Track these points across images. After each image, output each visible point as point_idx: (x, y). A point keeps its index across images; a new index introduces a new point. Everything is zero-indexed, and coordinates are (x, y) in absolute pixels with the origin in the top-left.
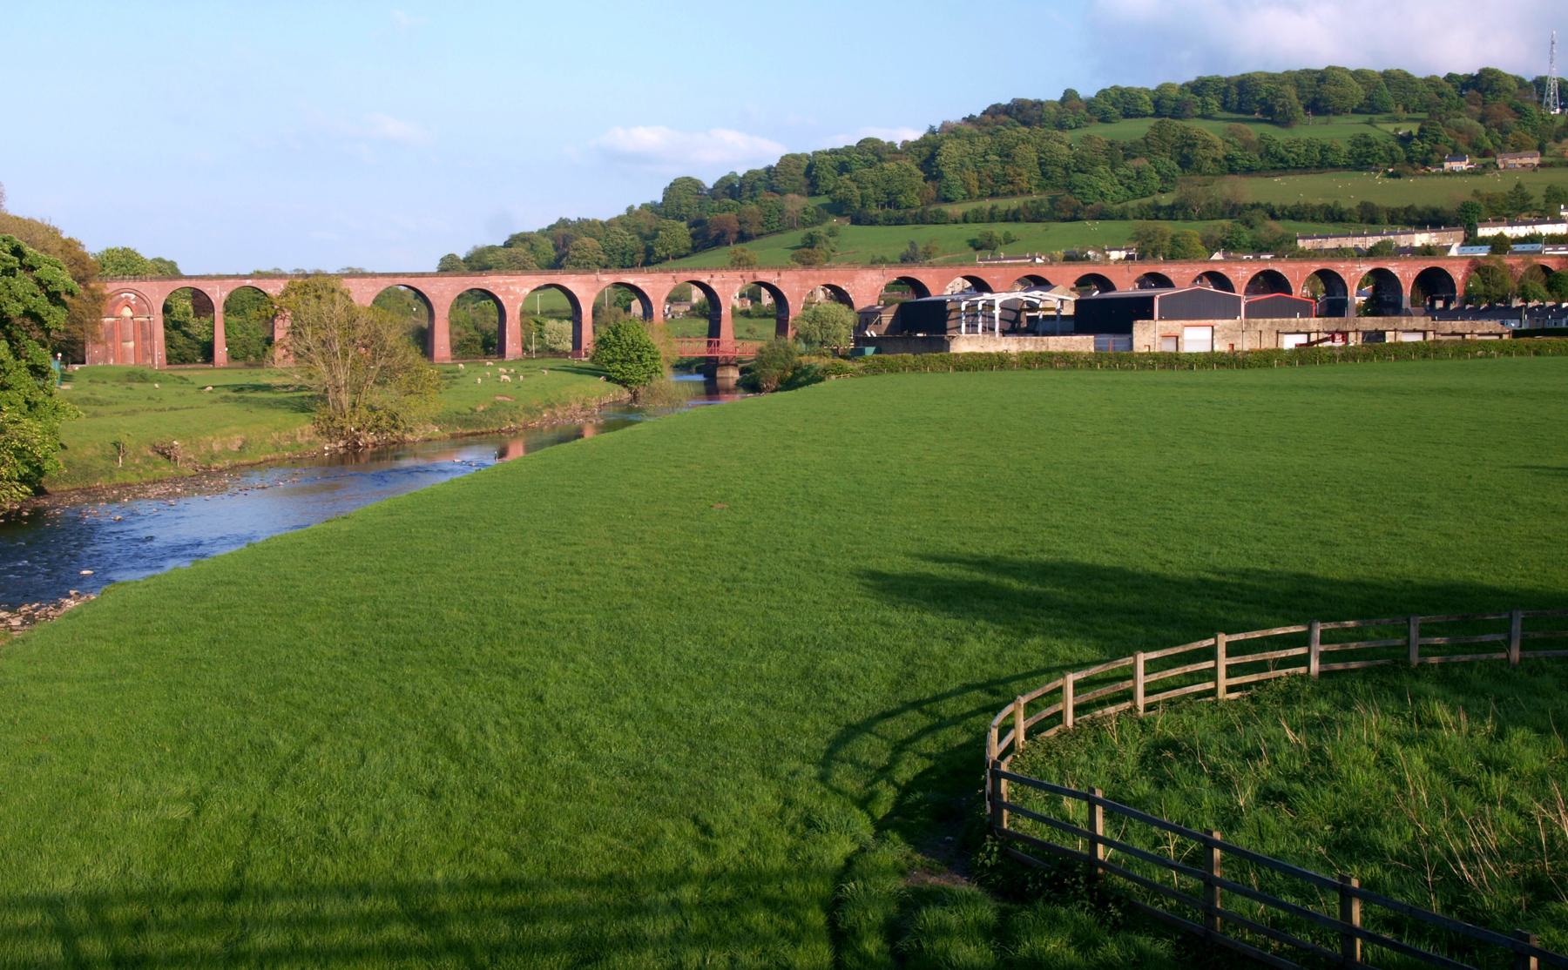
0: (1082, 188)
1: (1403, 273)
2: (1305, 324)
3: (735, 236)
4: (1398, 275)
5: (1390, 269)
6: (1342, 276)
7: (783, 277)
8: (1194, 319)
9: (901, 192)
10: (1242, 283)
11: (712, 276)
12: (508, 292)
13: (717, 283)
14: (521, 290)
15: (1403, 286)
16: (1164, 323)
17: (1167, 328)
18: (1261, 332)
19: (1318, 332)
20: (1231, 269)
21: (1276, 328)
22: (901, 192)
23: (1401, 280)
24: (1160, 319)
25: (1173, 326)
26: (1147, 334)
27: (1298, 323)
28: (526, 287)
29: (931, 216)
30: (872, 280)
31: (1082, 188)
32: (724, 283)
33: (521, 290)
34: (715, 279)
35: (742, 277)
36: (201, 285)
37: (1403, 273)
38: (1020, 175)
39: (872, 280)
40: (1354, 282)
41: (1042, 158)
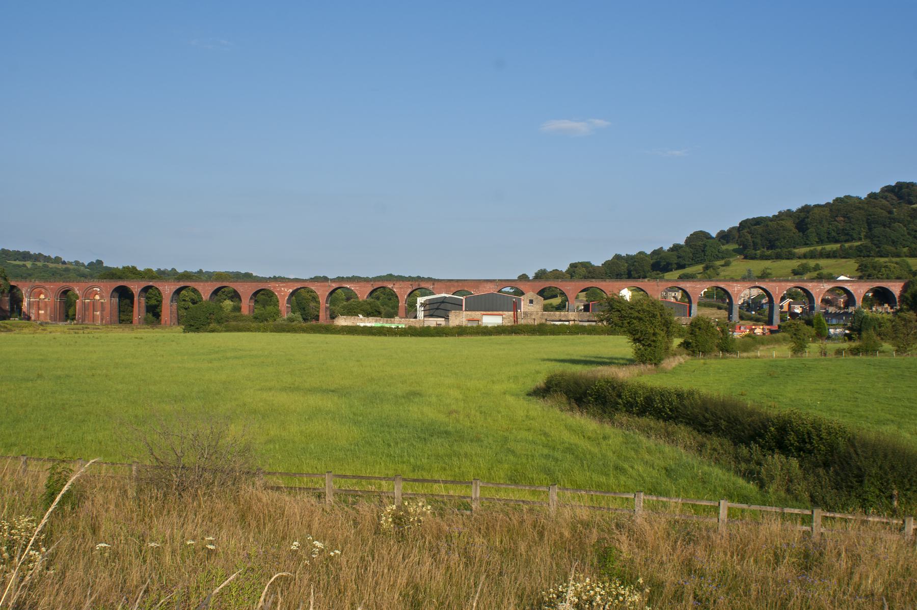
0: (879, 237)
1: (855, 290)
2: (565, 315)
3: (675, 266)
4: (852, 292)
5: (846, 287)
6: (810, 291)
7: (436, 286)
8: (493, 310)
9: (777, 240)
10: (284, 296)
11: (394, 284)
12: (280, 292)
13: (397, 288)
14: (287, 290)
15: (856, 298)
16: (469, 313)
17: (471, 315)
18: (534, 319)
19: (574, 320)
20: (729, 285)
21: (546, 317)
22: (777, 240)
23: (854, 294)
24: (466, 310)
25: (476, 314)
26: (458, 319)
27: (560, 315)
28: (290, 288)
29: (786, 255)
30: (490, 288)
31: (879, 237)
32: (401, 288)
33: (287, 290)
34: (396, 286)
35: (411, 285)
36: (270, 286)
37: (855, 290)
38: (853, 229)
39: (490, 288)
40: (819, 295)
41: (869, 219)
